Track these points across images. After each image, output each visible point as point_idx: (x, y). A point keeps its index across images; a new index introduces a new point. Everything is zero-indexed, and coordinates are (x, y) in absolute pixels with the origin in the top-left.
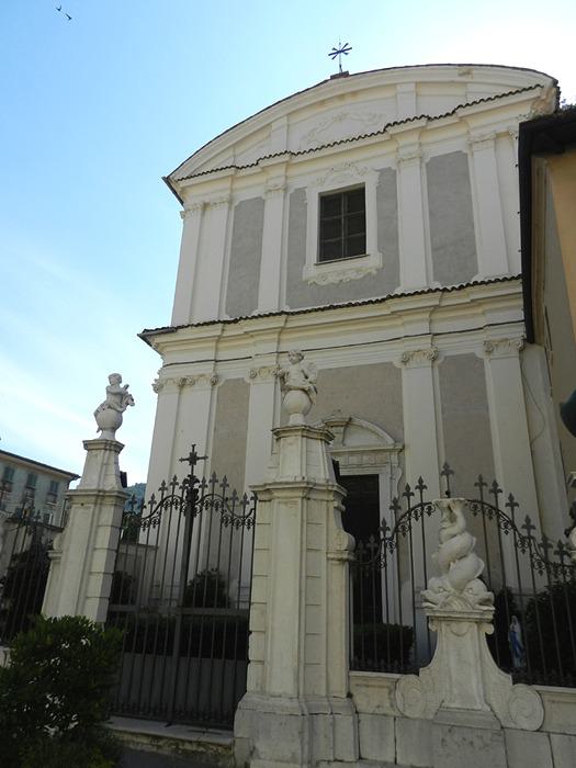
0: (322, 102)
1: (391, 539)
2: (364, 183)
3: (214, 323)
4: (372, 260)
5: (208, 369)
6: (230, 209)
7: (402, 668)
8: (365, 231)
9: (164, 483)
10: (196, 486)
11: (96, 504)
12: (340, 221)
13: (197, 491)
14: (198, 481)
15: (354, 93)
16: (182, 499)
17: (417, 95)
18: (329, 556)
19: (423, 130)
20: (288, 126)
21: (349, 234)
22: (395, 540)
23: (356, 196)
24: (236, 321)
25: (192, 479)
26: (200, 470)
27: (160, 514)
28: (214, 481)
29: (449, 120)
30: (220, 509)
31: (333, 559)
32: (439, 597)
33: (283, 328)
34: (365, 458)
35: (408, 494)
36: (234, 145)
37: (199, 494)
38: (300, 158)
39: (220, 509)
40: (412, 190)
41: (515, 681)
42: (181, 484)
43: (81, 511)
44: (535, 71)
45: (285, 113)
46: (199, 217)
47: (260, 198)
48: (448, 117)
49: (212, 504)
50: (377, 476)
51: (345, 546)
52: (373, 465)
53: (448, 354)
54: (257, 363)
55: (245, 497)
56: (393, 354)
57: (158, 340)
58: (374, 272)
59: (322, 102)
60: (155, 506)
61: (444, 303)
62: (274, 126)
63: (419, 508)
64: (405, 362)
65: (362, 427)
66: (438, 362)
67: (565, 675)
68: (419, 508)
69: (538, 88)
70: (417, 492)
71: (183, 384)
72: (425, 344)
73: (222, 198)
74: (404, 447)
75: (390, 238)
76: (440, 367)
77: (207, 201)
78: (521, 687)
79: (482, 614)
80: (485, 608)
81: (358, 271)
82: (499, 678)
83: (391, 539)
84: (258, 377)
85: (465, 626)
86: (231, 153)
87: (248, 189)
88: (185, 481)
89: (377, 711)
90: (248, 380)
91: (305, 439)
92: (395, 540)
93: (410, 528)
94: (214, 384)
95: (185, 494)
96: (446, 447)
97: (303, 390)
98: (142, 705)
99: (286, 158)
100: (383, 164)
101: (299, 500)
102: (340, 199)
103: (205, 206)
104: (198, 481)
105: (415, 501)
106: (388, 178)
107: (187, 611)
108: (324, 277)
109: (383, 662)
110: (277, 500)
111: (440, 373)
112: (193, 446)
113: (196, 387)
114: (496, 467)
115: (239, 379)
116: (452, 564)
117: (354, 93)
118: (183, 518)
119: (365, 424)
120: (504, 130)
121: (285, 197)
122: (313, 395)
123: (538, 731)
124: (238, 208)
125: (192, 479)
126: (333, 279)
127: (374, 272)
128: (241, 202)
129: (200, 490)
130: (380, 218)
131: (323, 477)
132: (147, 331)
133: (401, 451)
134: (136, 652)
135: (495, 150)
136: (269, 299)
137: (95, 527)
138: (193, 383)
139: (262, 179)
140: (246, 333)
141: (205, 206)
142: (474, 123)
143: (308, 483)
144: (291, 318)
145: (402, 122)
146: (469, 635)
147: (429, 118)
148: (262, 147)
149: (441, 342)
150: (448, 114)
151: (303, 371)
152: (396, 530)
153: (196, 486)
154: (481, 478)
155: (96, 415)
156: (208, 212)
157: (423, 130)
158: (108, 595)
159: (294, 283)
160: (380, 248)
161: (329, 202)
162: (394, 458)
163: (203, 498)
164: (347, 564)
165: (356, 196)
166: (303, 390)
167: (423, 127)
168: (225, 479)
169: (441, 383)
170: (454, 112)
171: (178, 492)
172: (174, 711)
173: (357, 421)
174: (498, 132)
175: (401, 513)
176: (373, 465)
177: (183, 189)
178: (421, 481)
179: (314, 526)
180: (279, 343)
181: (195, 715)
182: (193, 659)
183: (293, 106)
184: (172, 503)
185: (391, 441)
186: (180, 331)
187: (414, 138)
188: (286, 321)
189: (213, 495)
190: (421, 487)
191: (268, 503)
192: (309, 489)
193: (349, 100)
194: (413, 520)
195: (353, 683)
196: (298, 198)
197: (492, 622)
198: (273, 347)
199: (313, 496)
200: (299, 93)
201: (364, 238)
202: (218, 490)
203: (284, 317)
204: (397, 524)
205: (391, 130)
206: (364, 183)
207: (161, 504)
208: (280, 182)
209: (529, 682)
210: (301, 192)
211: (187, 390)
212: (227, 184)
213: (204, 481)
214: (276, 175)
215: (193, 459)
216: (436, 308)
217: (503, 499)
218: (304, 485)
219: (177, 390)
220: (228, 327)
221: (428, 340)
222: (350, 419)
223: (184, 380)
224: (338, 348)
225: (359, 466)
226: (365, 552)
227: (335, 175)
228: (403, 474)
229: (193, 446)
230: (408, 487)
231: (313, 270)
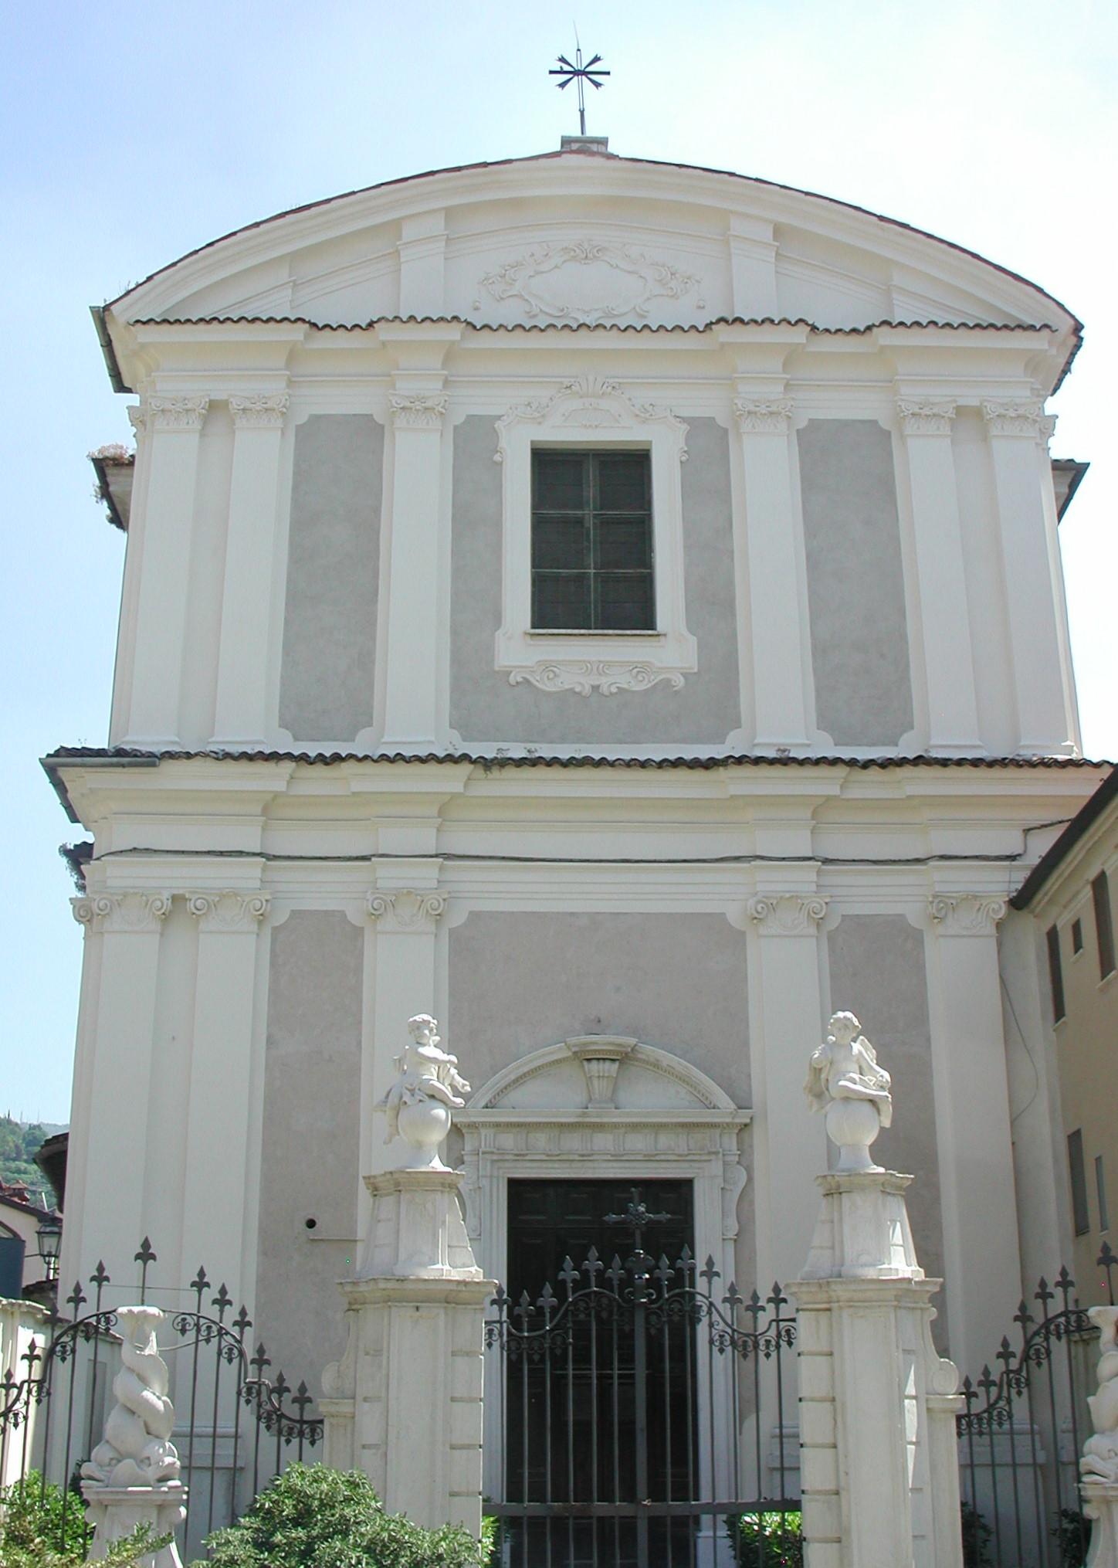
1: (1020, 1369)
4: (670, 650)
9: (1005, 1344)
22: (1024, 1373)
29: (853, 344)
34: (665, 1140)
35: (1044, 1295)
38: (486, 340)
40: (768, 483)
44: (1040, 290)
50: (689, 1183)
52: (681, 1159)
55: (755, 1297)
56: (723, 894)
58: (679, 682)
63: (1062, 1320)
68: (1062, 1320)
70: (1059, 1292)
75: (715, 603)
83: (1018, 1371)
92: (1024, 1373)
93: (73, 1351)
100: (707, 404)
102: (642, 508)
105: (1056, 1306)
106: (710, 443)
108: (547, 666)
119: (667, 1058)
120: (974, 402)
127: (679, 682)
130: (692, 543)
147: (814, 328)
152: (1026, 1358)
154: (202, 1274)
159: (470, 672)
160: (694, 622)
162: (731, 1142)
174: (962, 402)
175: (1033, 1327)
176: (681, 1159)
178: (202, 1274)
183: (468, 195)
186: (168, 766)
190: (100, 1278)
194: (1053, 1339)
196: (474, 442)
197: (761, 1514)
200: (485, 165)
204: (1028, 1343)
217: (231, 1314)
219: (156, 926)
223: (177, 900)
224: (594, 863)
225: (649, 1159)
228: (750, 1179)
230: (1043, 1284)
231: (518, 646)
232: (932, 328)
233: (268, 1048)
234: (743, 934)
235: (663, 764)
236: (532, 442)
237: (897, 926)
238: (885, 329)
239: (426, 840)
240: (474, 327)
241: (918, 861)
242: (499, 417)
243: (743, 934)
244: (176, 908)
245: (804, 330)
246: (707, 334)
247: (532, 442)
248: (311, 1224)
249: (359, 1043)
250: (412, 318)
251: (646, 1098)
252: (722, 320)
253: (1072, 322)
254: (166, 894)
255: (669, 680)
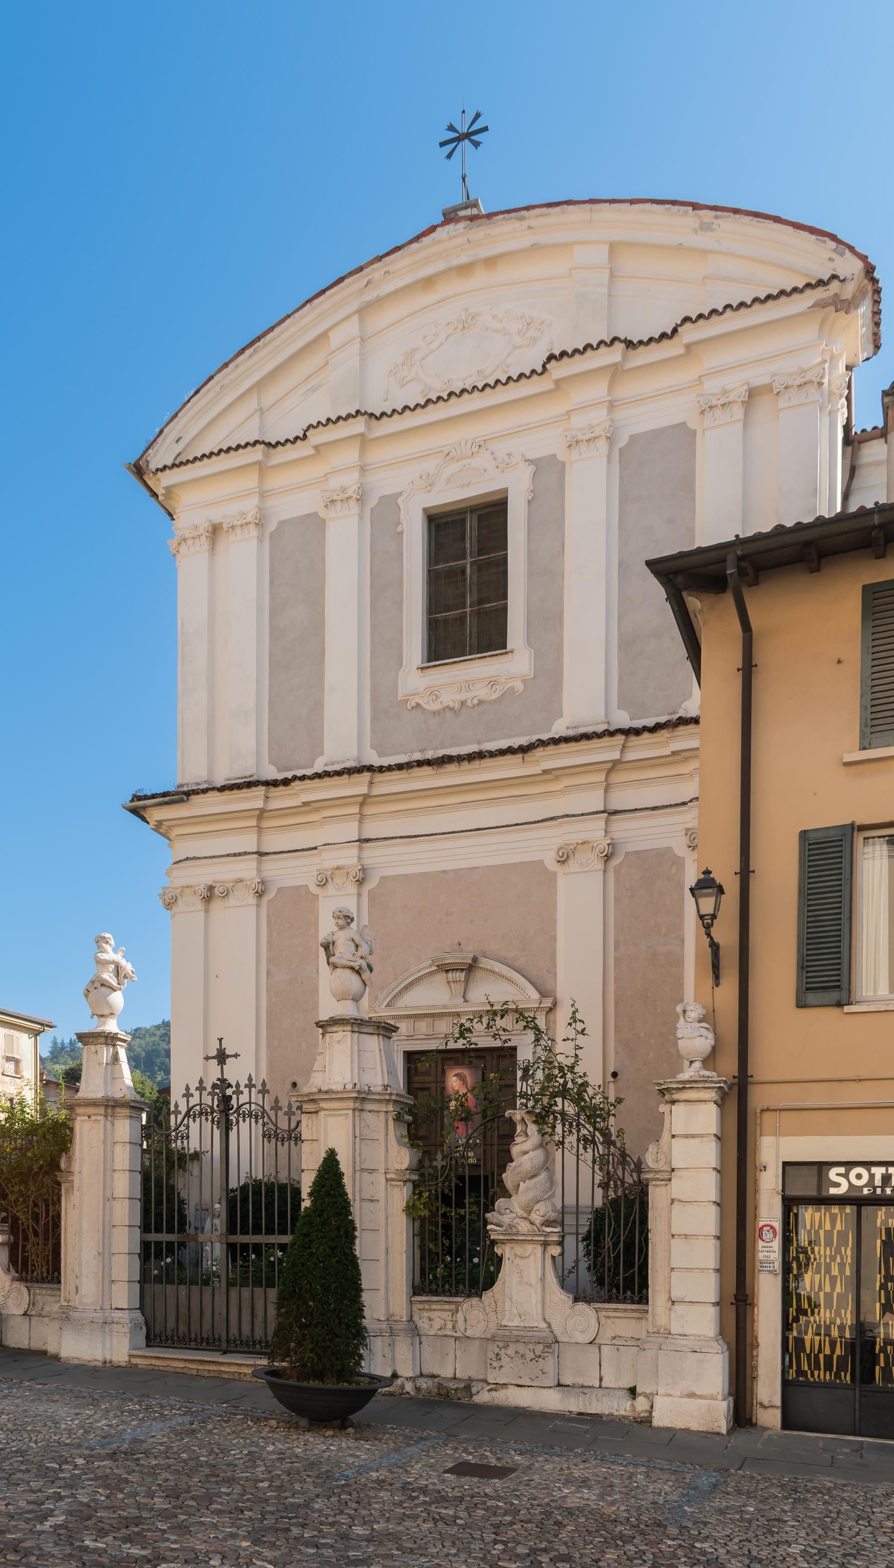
0: (428, 282)
2: (506, 490)
3: (249, 785)
4: (515, 664)
5: (247, 869)
6: (260, 540)
7: (453, 1291)
8: (505, 596)
10: (229, 1092)
11: (106, 1116)
12: (463, 572)
13: (231, 1097)
14: (230, 1086)
15: (491, 262)
16: (212, 1108)
17: (612, 275)
18: (388, 1176)
19: (615, 372)
20: (363, 340)
21: (480, 602)
23: (491, 514)
24: (286, 782)
25: (223, 1083)
26: (236, 1072)
27: (188, 1127)
28: (250, 1086)
30: (261, 1121)
31: (393, 1180)
32: (506, 1219)
33: (366, 797)
36: (259, 386)
37: (234, 1102)
39: (261, 1121)
41: (576, 1300)
42: (209, 1089)
43: (87, 1125)
45: (354, 306)
46: (206, 555)
47: (316, 514)
48: (665, 342)
49: (250, 1115)
51: (405, 1165)
53: (631, 848)
54: (328, 860)
56: (541, 846)
57: (156, 815)
58: (519, 686)
59: (428, 282)
60: (180, 1117)
61: (630, 756)
62: (336, 338)
64: (563, 861)
65: (493, 972)
66: (615, 862)
67: (624, 1292)
69: (835, 283)
71: (209, 895)
72: (594, 830)
73: (243, 514)
74: (555, 1004)
75: (549, 619)
76: (617, 871)
77: (216, 520)
78: (581, 1306)
79: (545, 1236)
80: (549, 1230)
81: (493, 683)
82: (560, 1298)
84: (330, 885)
85: (529, 1248)
86: (252, 404)
87: (297, 490)
88: (214, 1086)
89: (440, 1333)
90: (314, 890)
91: (356, 1035)
94: (260, 894)
95: (216, 1103)
96: (616, 1003)
97: (352, 968)
98: (193, 1336)
99: (358, 426)
101: (350, 1112)
102: (463, 521)
103: (215, 530)
104: (230, 1086)
106: (549, 472)
107: (233, 1239)
108: (433, 693)
109: (629, 1293)
110: (325, 1112)
111: (617, 881)
112: (220, 1040)
113: (232, 901)
114: (887, 933)
115: (298, 888)
116: (522, 1184)
117: (491, 262)
118: (217, 1133)
121: (361, 517)
122: (366, 975)
123: (591, 1343)
124: (275, 537)
125: (223, 1083)
126: (449, 698)
127: (519, 686)
128: (282, 523)
129: (234, 1097)
131: (379, 1082)
132: (140, 798)
133: (551, 1010)
134: (267, 1286)
135: (745, 427)
136: (343, 737)
137: (109, 1144)
138: (226, 895)
139: (315, 471)
140: (305, 804)
141: (215, 530)
142: (712, 359)
143: (359, 1092)
144: (379, 777)
145: (576, 351)
146: (532, 1257)
147: (629, 344)
148: (314, 390)
149: (622, 828)
150: (663, 336)
151: (353, 940)
153: (229, 1092)
155: (86, 996)
156: (223, 543)
157: (615, 372)
158: (138, 1221)
159: (383, 706)
161: (443, 526)
163: (239, 1107)
164: (410, 1185)
165: (491, 514)
166: (352, 968)
167: (615, 365)
168: (264, 1084)
169: (617, 900)
170: (675, 331)
171: (208, 1100)
172: (228, 1341)
173: (485, 963)
177: (169, 490)
179: (369, 1142)
180: (361, 821)
181: (251, 1343)
182: (268, 1290)
184: (201, 1114)
185: (535, 995)
187: (599, 390)
188: (371, 783)
189: (250, 1103)
191: (314, 1115)
192: (362, 1098)
193: (481, 278)
195: (414, 1308)
198: (351, 830)
199: (369, 1106)
201: (503, 611)
202: (256, 1097)
203: (366, 776)
205: (558, 370)
206: (506, 490)
207: (187, 1114)
208: (351, 480)
209: (588, 1301)
210: (390, 502)
211: (217, 905)
212: (251, 481)
213: (238, 1085)
214: (341, 468)
215: (222, 1057)
216: (615, 766)
218: (355, 1095)
219: (200, 906)
220: (274, 791)
221: (599, 823)
222: (475, 959)
223: (211, 888)
226: (432, 1171)
227: (455, 467)
229: (220, 1040)
232: (729, 312)
233: (267, 979)
234: (556, 873)
235: (502, 752)
236: (425, 510)
237: (301, 892)
238: (688, 325)
239: (248, 842)
240: (376, 418)
241: (684, 804)
242: (400, 494)
243: (556, 873)
244: (209, 895)
245: (619, 347)
246: (676, 339)
247: (425, 510)
248: (294, 1085)
249: (318, 970)
250: (522, 375)
251: (488, 991)
252: (687, 319)
253: (860, 264)
254: (203, 886)
255: (513, 688)
